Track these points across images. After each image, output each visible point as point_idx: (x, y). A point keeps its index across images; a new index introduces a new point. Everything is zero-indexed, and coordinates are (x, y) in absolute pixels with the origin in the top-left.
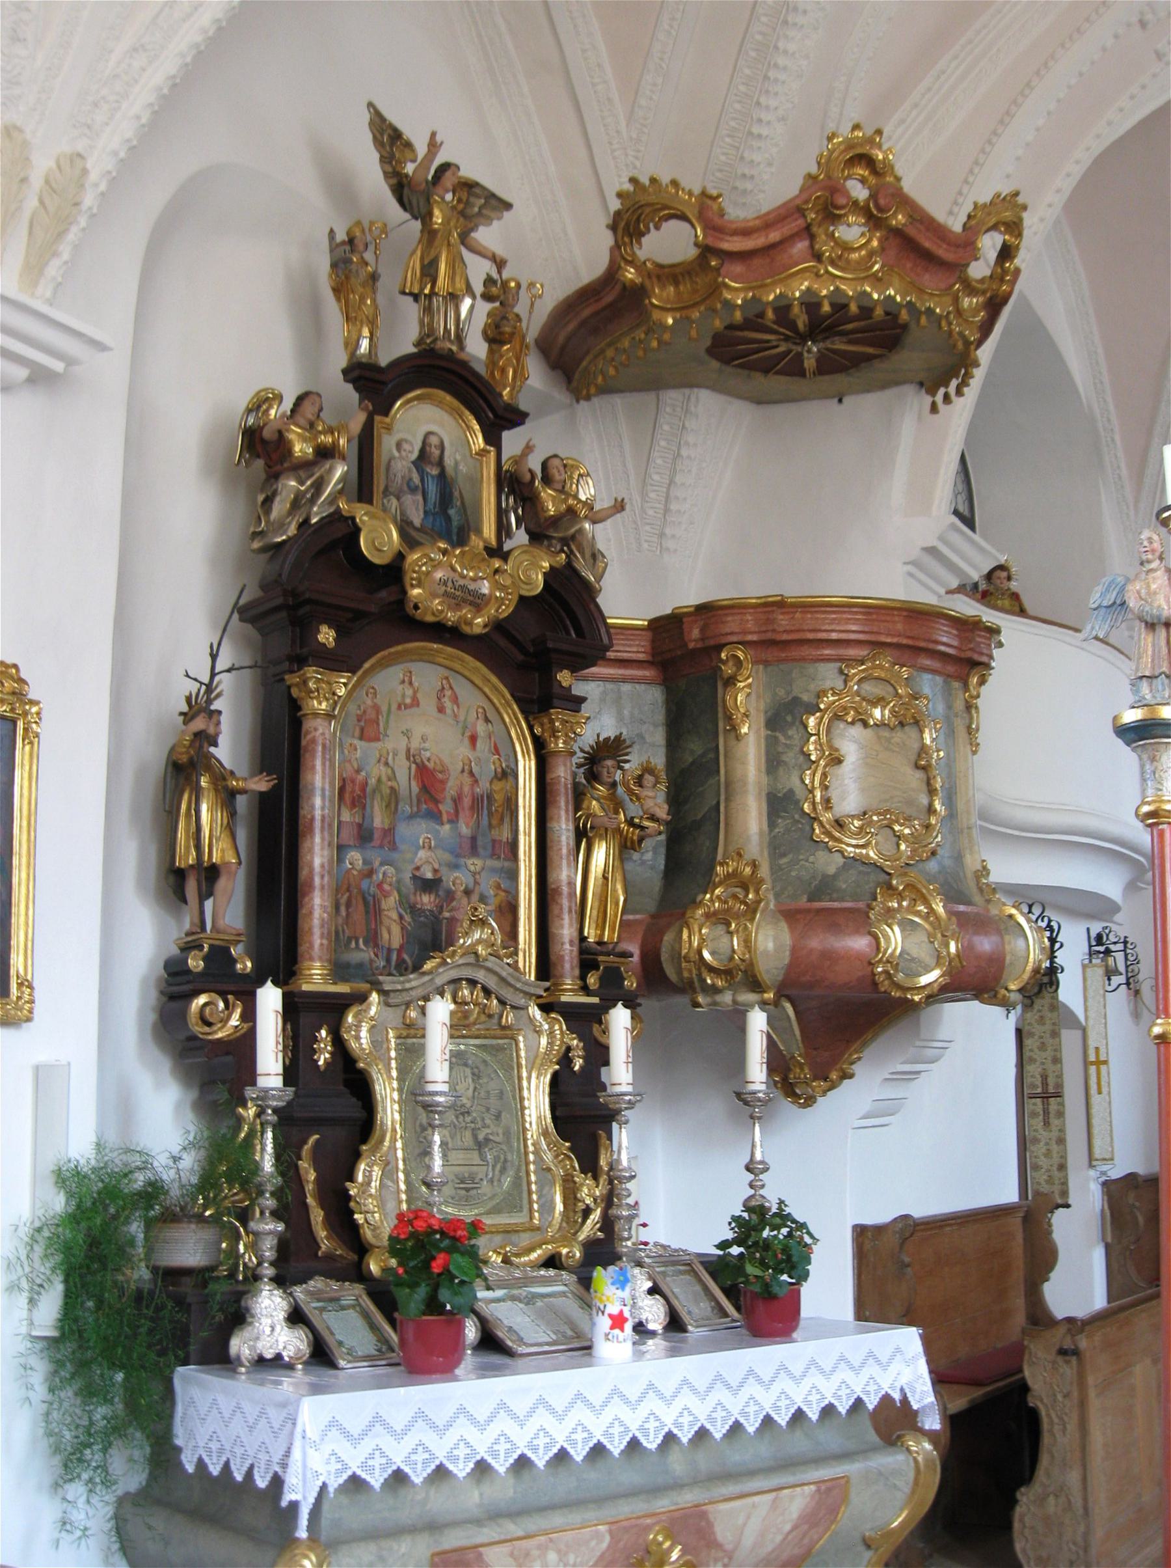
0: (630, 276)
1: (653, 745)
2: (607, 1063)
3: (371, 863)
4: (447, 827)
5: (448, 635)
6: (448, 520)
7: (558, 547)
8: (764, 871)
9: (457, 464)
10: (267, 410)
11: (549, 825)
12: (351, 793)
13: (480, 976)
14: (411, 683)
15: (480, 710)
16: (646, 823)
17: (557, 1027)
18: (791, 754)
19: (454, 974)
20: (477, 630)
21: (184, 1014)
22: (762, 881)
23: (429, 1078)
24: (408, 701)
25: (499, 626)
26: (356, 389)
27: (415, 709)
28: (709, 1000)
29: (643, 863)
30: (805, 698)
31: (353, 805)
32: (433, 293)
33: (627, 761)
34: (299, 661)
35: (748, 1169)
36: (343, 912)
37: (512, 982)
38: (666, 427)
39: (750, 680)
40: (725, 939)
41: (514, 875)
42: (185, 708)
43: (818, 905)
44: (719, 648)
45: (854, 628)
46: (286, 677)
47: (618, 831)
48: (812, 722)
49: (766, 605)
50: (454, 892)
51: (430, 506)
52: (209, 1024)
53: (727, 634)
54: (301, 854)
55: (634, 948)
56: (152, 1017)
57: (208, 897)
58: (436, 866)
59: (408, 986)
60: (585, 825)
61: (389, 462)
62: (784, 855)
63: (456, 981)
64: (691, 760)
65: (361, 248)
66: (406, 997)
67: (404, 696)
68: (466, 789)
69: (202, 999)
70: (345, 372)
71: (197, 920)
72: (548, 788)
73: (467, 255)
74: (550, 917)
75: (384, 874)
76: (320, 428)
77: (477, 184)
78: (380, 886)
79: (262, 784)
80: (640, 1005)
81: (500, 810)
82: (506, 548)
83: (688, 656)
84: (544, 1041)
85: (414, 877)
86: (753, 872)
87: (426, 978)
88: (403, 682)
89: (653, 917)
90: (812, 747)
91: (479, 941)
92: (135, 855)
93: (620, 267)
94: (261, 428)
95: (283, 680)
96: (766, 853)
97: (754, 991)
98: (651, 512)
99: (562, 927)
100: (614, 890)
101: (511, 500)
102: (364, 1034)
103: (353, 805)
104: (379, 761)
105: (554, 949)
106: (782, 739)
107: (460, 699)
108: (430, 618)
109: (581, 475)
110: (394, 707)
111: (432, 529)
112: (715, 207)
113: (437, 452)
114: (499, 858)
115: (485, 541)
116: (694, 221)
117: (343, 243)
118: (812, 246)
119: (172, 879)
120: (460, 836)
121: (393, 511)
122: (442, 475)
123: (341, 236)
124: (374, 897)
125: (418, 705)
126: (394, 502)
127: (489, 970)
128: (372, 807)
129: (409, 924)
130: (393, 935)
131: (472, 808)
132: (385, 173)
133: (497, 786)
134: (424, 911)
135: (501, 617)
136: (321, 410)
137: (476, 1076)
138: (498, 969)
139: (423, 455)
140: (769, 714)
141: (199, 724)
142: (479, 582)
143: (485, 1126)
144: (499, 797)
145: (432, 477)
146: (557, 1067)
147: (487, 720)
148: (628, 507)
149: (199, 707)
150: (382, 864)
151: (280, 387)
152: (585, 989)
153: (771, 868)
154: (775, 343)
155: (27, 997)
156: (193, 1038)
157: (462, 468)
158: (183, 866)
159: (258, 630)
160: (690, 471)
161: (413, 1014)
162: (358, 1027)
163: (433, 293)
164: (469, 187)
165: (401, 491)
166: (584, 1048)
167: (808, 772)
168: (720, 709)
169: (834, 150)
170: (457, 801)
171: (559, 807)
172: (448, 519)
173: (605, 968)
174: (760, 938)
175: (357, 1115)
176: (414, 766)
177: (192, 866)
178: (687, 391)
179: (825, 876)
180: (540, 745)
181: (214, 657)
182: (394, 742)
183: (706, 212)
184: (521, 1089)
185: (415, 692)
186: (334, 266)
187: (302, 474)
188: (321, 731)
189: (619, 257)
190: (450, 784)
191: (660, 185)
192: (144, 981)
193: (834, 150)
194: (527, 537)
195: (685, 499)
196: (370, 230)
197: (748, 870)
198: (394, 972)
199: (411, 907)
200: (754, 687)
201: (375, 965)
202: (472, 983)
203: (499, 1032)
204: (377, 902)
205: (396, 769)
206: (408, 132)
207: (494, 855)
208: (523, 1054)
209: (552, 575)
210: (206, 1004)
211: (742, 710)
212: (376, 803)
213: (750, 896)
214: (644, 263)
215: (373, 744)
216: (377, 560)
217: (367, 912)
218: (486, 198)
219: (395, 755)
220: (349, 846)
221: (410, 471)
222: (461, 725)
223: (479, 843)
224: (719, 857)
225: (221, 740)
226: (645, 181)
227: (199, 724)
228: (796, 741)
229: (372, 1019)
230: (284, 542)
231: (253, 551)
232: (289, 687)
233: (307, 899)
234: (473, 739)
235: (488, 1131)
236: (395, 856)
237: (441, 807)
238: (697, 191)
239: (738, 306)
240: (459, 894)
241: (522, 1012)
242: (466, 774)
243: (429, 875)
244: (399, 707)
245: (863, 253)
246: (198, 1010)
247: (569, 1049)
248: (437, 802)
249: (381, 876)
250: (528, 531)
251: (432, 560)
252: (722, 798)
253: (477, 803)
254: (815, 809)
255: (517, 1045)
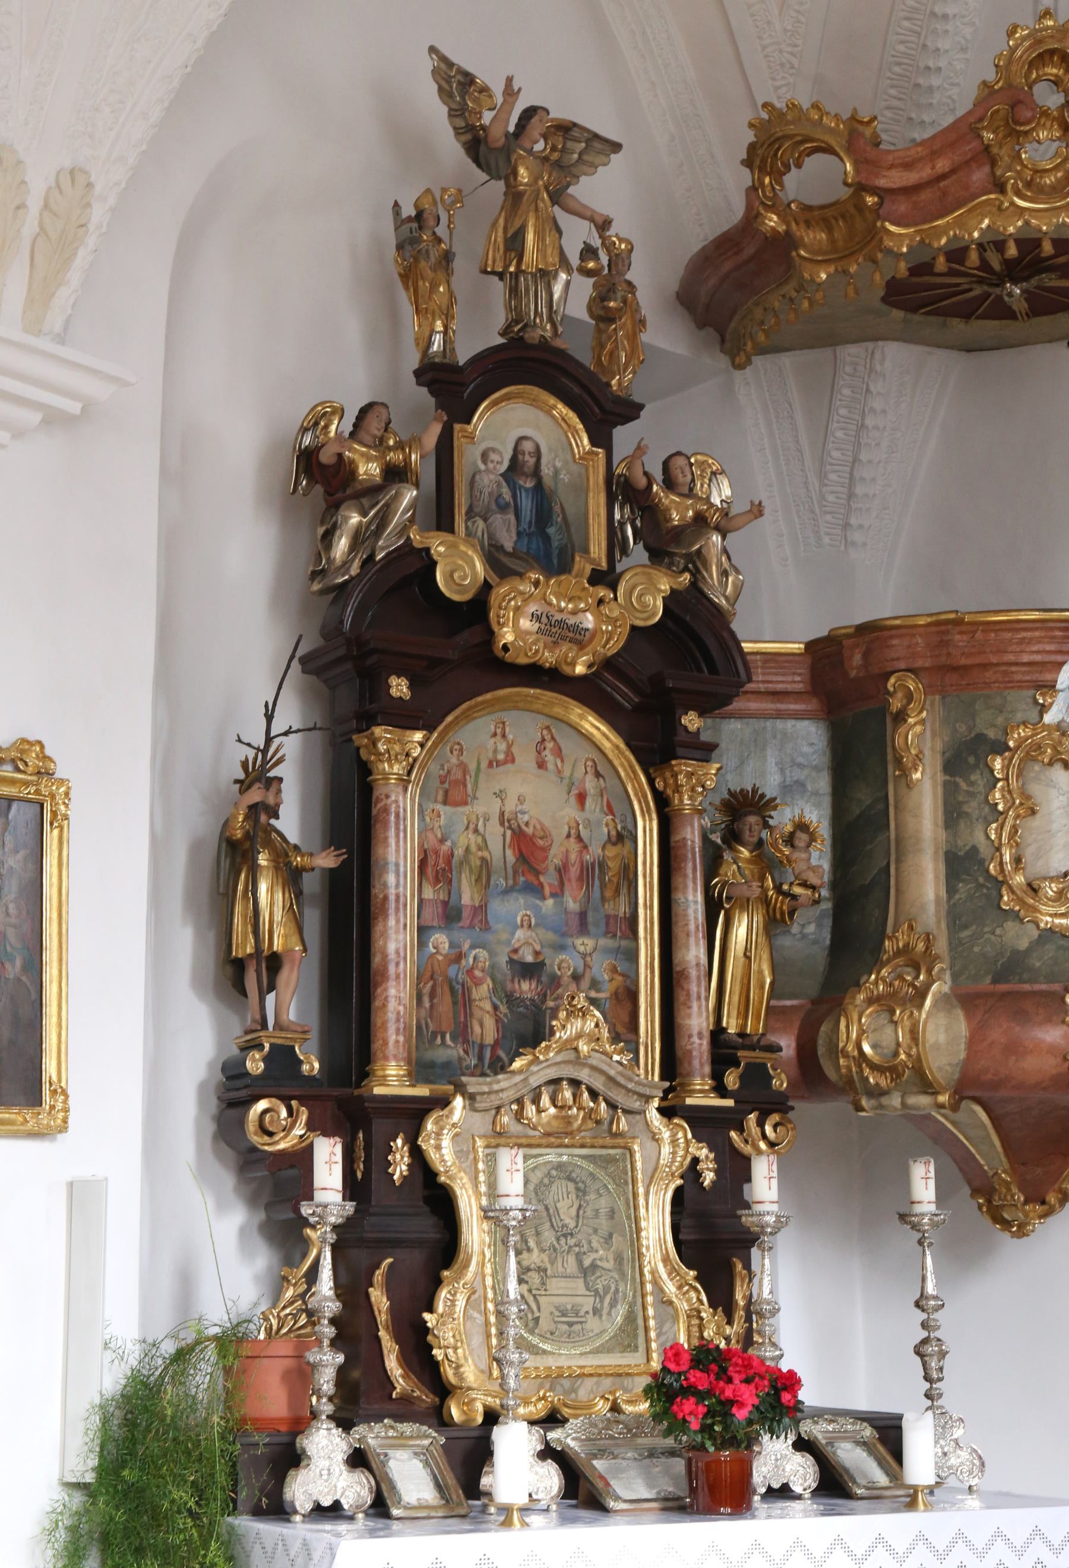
0: (772, 224)
1: (816, 793)
2: (749, 1179)
3: (460, 947)
4: (550, 902)
5: (546, 679)
6: (542, 543)
7: (681, 566)
8: (941, 946)
9: (556, 472)
10: (326, 427)
11: (673, 896)
12: (435, 866)
13: (584, 1075)
14: (504, 736)
15: (589, 763)
16: (797, 890)
17: (680, 1135)
18: (974, 804)
19: (552, 1073)
20: (580, 670)
21: (242, 1122)
22: (937, 958)
23: (916, 1198)
24: (501, 757)
25: (608, 665)
26: (432, 393)
27: (509, 766)
28: (873, 1102)
29: (804, 936)
30: (991, 734)
31: (437, 881)
32: (519, 271)
33: (772, 818)
34: (367, 720)
35: (917, 1305)
36: (427, 1004)
37: (622, 1081)
38: (846, 392)
39: (924, 714)
40: (889, 1030)
41: (632, 956)
42: (241, 775)
43: (1003, 987)
44: (888, 675)
45: (1049, 647)
46: (354, 737)
47: (765, 901)
48: (998, 764)
49: (938, 623)
50: (560, 978)
51: (524, 526)
52: (271, 1134)
53: (893, 660)
54: (373, 939)
55: (787, 1044)
56: (211, 1128)
57: (270, 991)
58: (538, 948)
59: (496, 1087)
60: (720, 894)
61: (474, 476)
62: (966, 927)
63: (556, 1082)
64: (858, 812)
65: (431, 222)
66: (495, 1100)
67: (495, 751)
68: (573, 857)
69: (262, 1105)
70: (418, 373)
71: (258, 1017)
72: (672, 853)
73: (563, 218)
74: (676, 1006)
75: (475, 958)
76: (391, 442)
77: (575, 125)
78: (470, 972)
79: (328, 860)
80: (792, 1108)
81: (615, 880)
82: (619, 568)
83: (848, 686)
84: (666, 1150)
85: (511, 961)
86: (927, 948)
87: (518, 1078)
88: (495, 735)
89: (814, 1002)
90: (998, 795)
91: (579, 1036)
92: (186, 944)
93: (758, 214)
94: (318, 449)
95: (350, 740)
96: (943, 925)
97: (926, 1093)
98: (831, 498)
99: (689, 1016)
100: (760, 972)
101: (627, 510)
102: (446, 1142)
103: (437, 881)
104: (467, 828)
105: (682, 1043)
106: (963, 786)
107: (564, 752)
108: (522, 660)
109: (714, 473)
110: (484, 765)
111: (528, 553)
112: (868, 132)
113: (531, 461)
114: (615, 936)
115: (592, 561)
116: (842, 154)
117: (409, 219)
118: (993, 173)
119: (229, 970)
120: (566, 912)
121: (479, 534)
122: (539, 486)
123: (408, 210)
124: (463, 985)
125: (513, 761)
126: (481, 524)
127: (594, 1068)
128: (459, 881)
129: (505, 1015)
130: (486, 1029)
131: (580, 879)
132: (455, 128)
133: (612, 851)
134: (523, 1000)
135: (609, 654)
136: (389, 422)
137: (581, 1192)
138: (605, 1068)
139: (515, 465)
140: (947, 755)
141: (255, 795)
142: (581, 615)
143: (592, 1250)
144: (613, 865)
145: (527, 490)
146: (679, 1182)
147: (598, 775)
148: (766, 511)
149: (258, 775)
150: (473, 947)
151: (339, 400)
152: (720, 1090)
153: (950, 944)
154: (966, 287)
155: (59, 1106)
156: (254, 1149)
157: (563, 476)
158: (240, 956)
159: (325, 681)
160: (878, 444)
161: (505, 1119)
162: (439, 1134)
163: (519, 271)
164: (565, 129)
165: (488, 510)
166: (716, 1160)
167: (994, 825)
168: (889, 750)
169: (1016, 47)
170: (562, 871)
171: (685, 876)
172: (547, 539)
173: (747, 1065)
174: (930, 1027)
175: (433, 1236)
176: (509, 833)
177: (251, 955)
178: (870, 345)
179: (1015, 953)
180: (663, 803)
181: (269, 717)
182: (485, 806)
183: (858, 138)
184: (636, 1208)
185: (509, 746)
186: (400, 247)
187: (365, 501)
188: (393, 798)
189: (757, 200)
190: (552, 852)
191: (801, 109)
192: (202, 1087)
193: (1016, 47)
194: (646, 555)
195: (873, 480)
196: (442, 198)
197: (921, 946)
198: (488, 1071)
199: (506, 996)
200: (928, 725)
201: (465, 1064)
202: (575, 1083)
203: (608, 1141)
204: (466, 991)
205: (487, 836)
206: (483, 76)
207: (609, 933)
208: (639, 1165)
209: (672, 600)
210: (265, 1112)
211: (913, 752)
212: (463, 876)
213: (921, 977)
214: (789, 205)
215: (461, 809)
216: (456, 598)
217: (455, 1003)
218: (587, 141)
219: (486, 819)
220: (433, 927)
221: (499, 485)
222: (566, 782)
223: (590, 917)
224: (889, 930)
225: (282, 811)
226: (780, 105)
227: (255, 795)
228: (981, 788)
229: (454, 1125)
230: (346, 583)
231: (314, 593)
232: (358, 749)
233: (379, 990)
234: (582, 798)
235: (593, 1256)
236: (490, 937)
237: (542, 878)
238: (845, 116)
239: (902, 254)
240: (565, 980)
241: (638, 1117)
242: (572, 840)
243: (529, 959)
244: (490, 765)
245: (1059, 175)
246: (256, 1118)
247: (696, 1161)
248: (537, 873)
249: (471, 961)
250: (647, 548)
251: (522, 593)
252: (893, 858)
253: (587, 873)
254: (1002, 870)
255: (632, 1155)
